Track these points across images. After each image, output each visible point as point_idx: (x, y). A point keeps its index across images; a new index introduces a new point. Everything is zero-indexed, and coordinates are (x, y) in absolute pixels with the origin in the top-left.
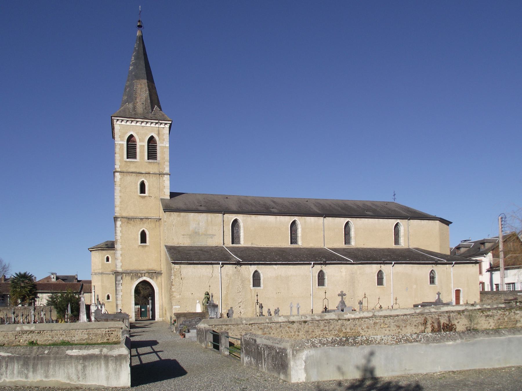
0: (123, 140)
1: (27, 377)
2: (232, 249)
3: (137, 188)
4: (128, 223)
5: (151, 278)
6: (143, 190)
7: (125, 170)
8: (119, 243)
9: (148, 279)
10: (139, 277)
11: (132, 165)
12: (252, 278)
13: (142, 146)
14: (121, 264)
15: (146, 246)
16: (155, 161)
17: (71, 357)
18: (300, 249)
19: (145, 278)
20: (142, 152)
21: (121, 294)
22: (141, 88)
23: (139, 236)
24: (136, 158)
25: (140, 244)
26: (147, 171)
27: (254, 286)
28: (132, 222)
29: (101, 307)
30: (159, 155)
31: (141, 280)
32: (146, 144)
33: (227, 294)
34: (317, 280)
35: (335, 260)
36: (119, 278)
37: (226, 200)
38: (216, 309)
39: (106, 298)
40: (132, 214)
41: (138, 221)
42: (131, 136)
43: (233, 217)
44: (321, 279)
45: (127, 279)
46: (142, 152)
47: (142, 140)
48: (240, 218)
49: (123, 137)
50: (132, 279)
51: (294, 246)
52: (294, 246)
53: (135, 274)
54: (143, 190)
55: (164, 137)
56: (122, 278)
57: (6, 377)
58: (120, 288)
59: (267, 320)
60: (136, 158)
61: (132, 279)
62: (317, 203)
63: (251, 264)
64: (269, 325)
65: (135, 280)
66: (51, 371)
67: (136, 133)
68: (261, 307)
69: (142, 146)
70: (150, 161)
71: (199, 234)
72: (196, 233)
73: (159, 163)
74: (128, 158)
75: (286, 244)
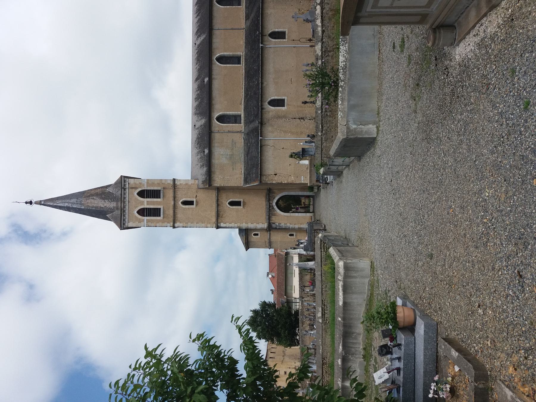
0: (143, 220)
1: (359, 334)
2: (247, 123)
3: (189, 208)
4: (222, 217)
5: (274, 198)
6: (191, 203)
7: (172, 219)
8: (241, 225)
9: (275, 201)
10: (273, 208)
11: (167, 212)
12: (276, 108)
13: (147, 203)
14: (261, 224)
15: (244, 202)
16: (162, 192)
17: (345, 303)
18: (246, 55)
19: (274, 204)
20: (153, 203)
21: (288, 225)
22: (91, 203)
23: (234, 207)
24: (160, 209)
25: (242, 207)
26: (172, 199)
27: (284, 106)
28: (221, 214)
29: (302, 243)
30: (156, 188)
31: (275, 207)
32: (146, 200)
33: (293, 133)
34: (279, 40)
35: (258, 20)
36: (274, 226)
37: (197, 127)
38: (306, 150)
39: (292, 237)
40: (214, 213)
41: (220, 208)
42: (138, 212)
43: (215, 122)
44: (280, 35)
45: (274, 219)
46: (153, 203)
47: (142, 203)
48: (216, 115)
49: (140, 219)
50: (275, 215)
51: (243, 60)
52: (243, 60)
53: (270, 213)
54: (191, 203)
55: (137, 183)
56: (274, 223)
57: (359, 348)
58: (283, 225)
59: (320, 112)
60: (160, 209)
61: (275, 215)
62: (198, 32)
63: (262, 109)
64: (324, 111)
65: (275, 212)
66: (357, 331)
67: (138, 200)
68: (305, 103)
69: (147, 203)
70: (162, 196)
71: (232, 155)
72: (230, 158)
73: (164, 188)
74: (160, 216)
75: (241, 68)
